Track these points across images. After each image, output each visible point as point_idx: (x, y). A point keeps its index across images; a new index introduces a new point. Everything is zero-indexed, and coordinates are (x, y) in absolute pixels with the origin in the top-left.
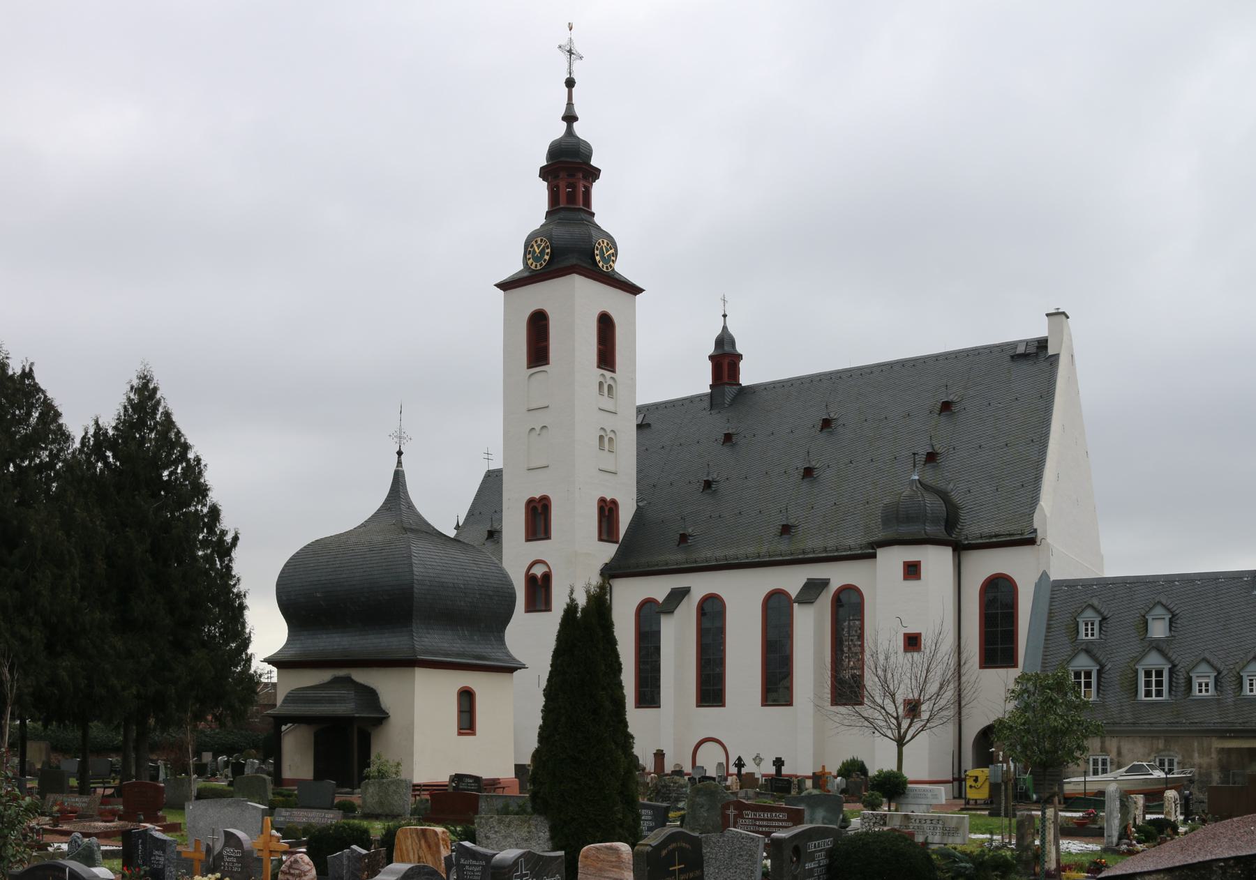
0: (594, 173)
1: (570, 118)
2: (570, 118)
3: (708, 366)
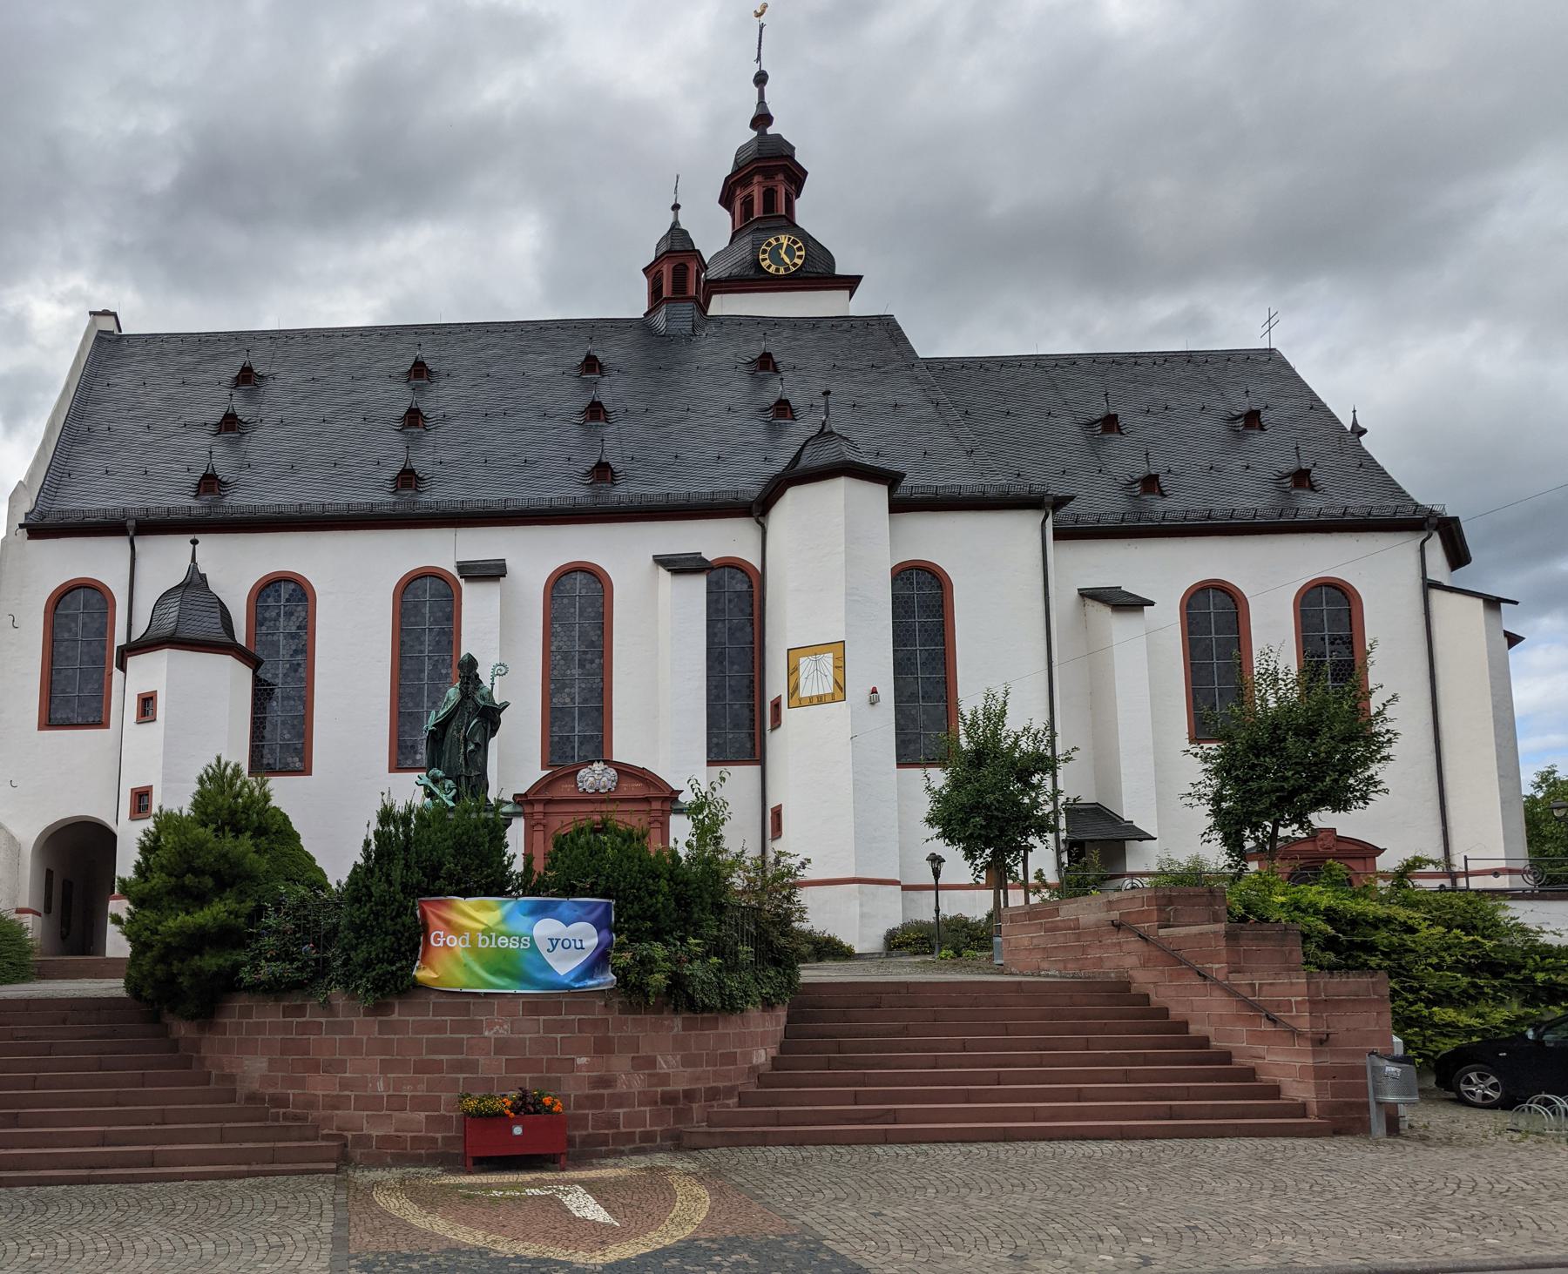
0: (797, 177)
1: (762, 119)
2: (762, 119)
3: (643, 283)
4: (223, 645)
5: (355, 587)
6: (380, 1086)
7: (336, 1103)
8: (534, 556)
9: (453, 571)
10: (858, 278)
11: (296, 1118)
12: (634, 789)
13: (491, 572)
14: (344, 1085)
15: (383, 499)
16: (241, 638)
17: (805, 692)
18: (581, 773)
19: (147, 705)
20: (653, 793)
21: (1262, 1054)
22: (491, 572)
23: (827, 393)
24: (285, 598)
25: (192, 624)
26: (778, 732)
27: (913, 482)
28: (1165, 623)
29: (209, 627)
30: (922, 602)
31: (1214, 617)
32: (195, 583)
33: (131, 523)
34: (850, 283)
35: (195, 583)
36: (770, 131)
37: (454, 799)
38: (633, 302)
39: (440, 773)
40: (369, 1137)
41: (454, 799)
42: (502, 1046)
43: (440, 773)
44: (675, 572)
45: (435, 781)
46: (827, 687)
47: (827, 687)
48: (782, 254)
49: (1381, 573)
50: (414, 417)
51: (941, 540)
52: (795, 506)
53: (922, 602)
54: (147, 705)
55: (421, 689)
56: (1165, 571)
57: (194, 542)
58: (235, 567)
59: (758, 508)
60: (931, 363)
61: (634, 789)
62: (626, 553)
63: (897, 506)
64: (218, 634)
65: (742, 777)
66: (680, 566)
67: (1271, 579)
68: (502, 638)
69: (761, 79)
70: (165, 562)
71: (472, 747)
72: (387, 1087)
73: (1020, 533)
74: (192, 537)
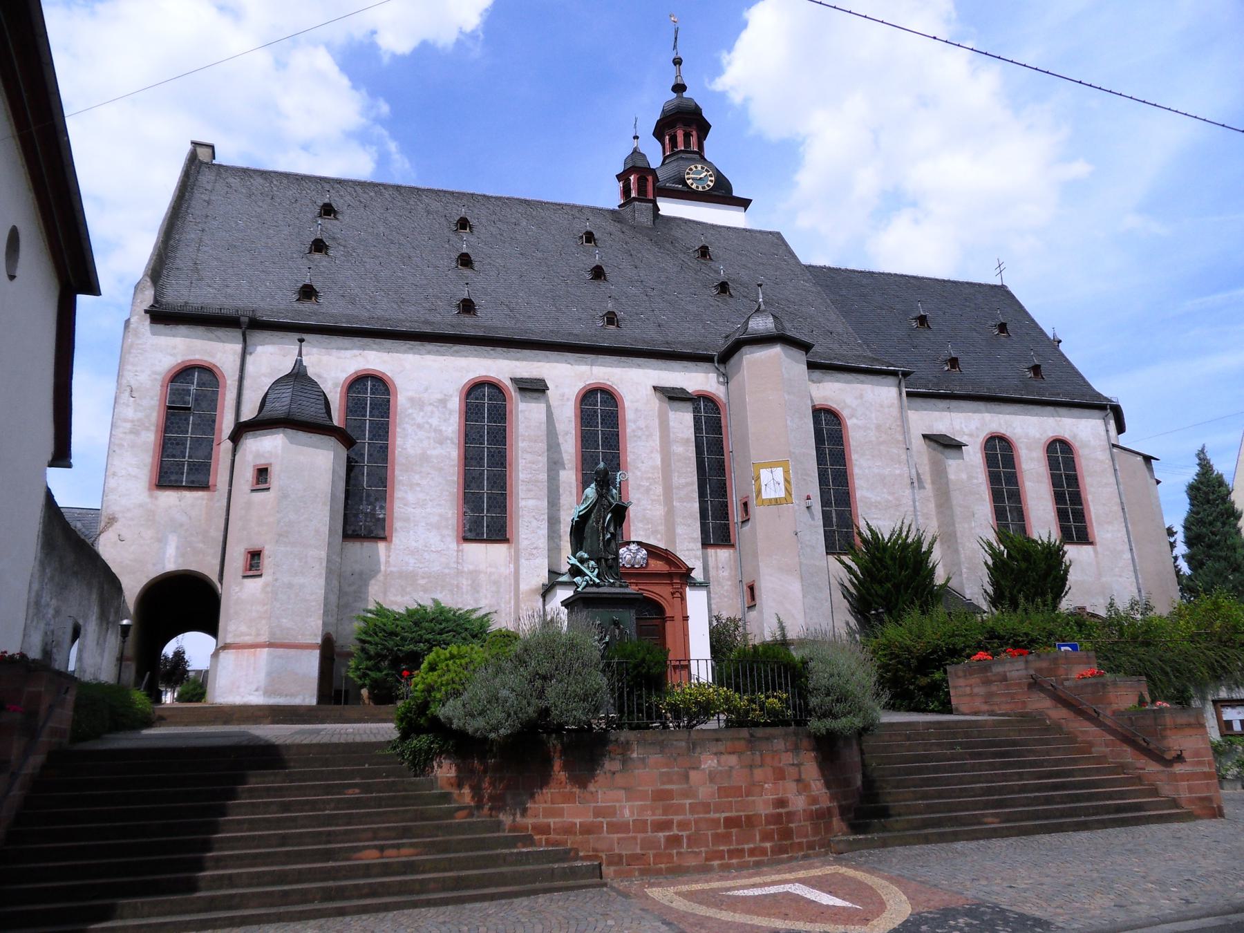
0: (704, 128)
1: (679, 88)
2: (679, 88)
4: (318, 427)
5: (429, 387)
6: (627, 813)
7: (588, 830)
8: (567, 378)
9: (508, 383)
10: (750, 201)
11: (557, 843)
12: (657, 566)
13: (534, 388)
14: (598, 813)
15: (448, 320)
16: (337, 420)
17: (765, 496)
18: (621, 551)
19: (262, 473)
20: (673, 570)
21: (677, 897)
22: (534, 388)
23: (954, 362)
24: (371, 393)
25: (295, 410)
26: (747, 528)
27: (822, 350)
28: (974, 456)
29: (311, 411)
30: (828, 428)
31: (1000, 453)
32: (298, 376)
33: (244, 320)
34: (744, 203)
35: (298, 376)
36: (685, 95)
37: (598, 576)
38: (611, 197)
39: (586, 556)
40: (620, 856)
41: (598, 576)
42: (712, 777)
43: (586, 556)
44: (671, 399)
45: (582, 561)
46: (781, 494)
47: (781, 494)
48: (698, 177)
49: (1085, 431)
50: (319, 246)
51: (834, 392)
52: (753, 358)
53: (828, 428)
54: (262, 473)
55: (482, 474)
56: (971, 424)
57: (301, 341)
58: (334, 366)
59: (723, 359)
60: (811, 268)
61: (657, 566)
62: (635, 383)
63: (812, 366)
64: (321, 418)
65: (721, 556)
66: (674, 396)
67: (1030, 430)
68: (542, 435)
69: (677, 62)
70: (271, 359)
71: (609, 536)
72: (632, 813)
73: (885, 394)
74: (297, 336)
